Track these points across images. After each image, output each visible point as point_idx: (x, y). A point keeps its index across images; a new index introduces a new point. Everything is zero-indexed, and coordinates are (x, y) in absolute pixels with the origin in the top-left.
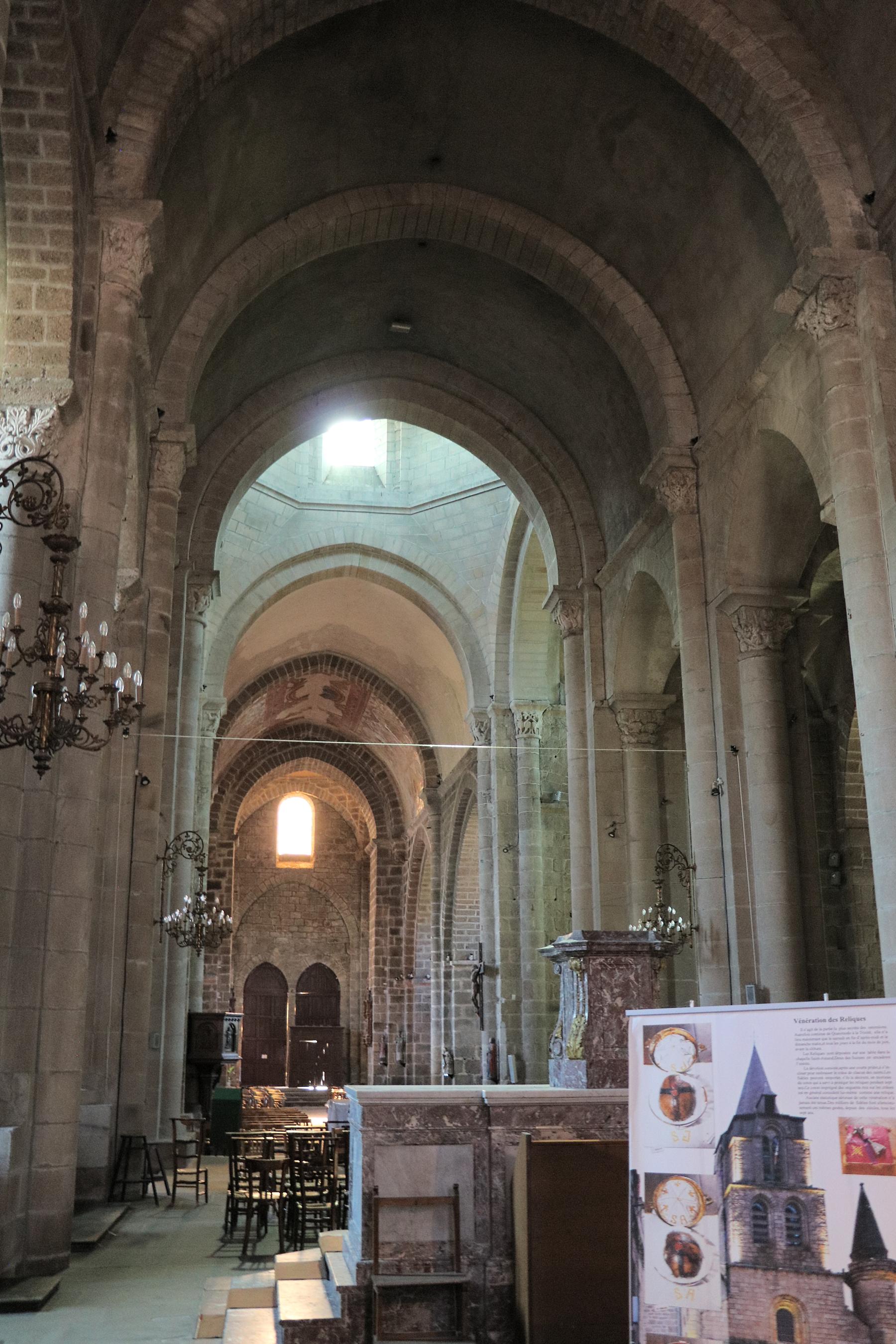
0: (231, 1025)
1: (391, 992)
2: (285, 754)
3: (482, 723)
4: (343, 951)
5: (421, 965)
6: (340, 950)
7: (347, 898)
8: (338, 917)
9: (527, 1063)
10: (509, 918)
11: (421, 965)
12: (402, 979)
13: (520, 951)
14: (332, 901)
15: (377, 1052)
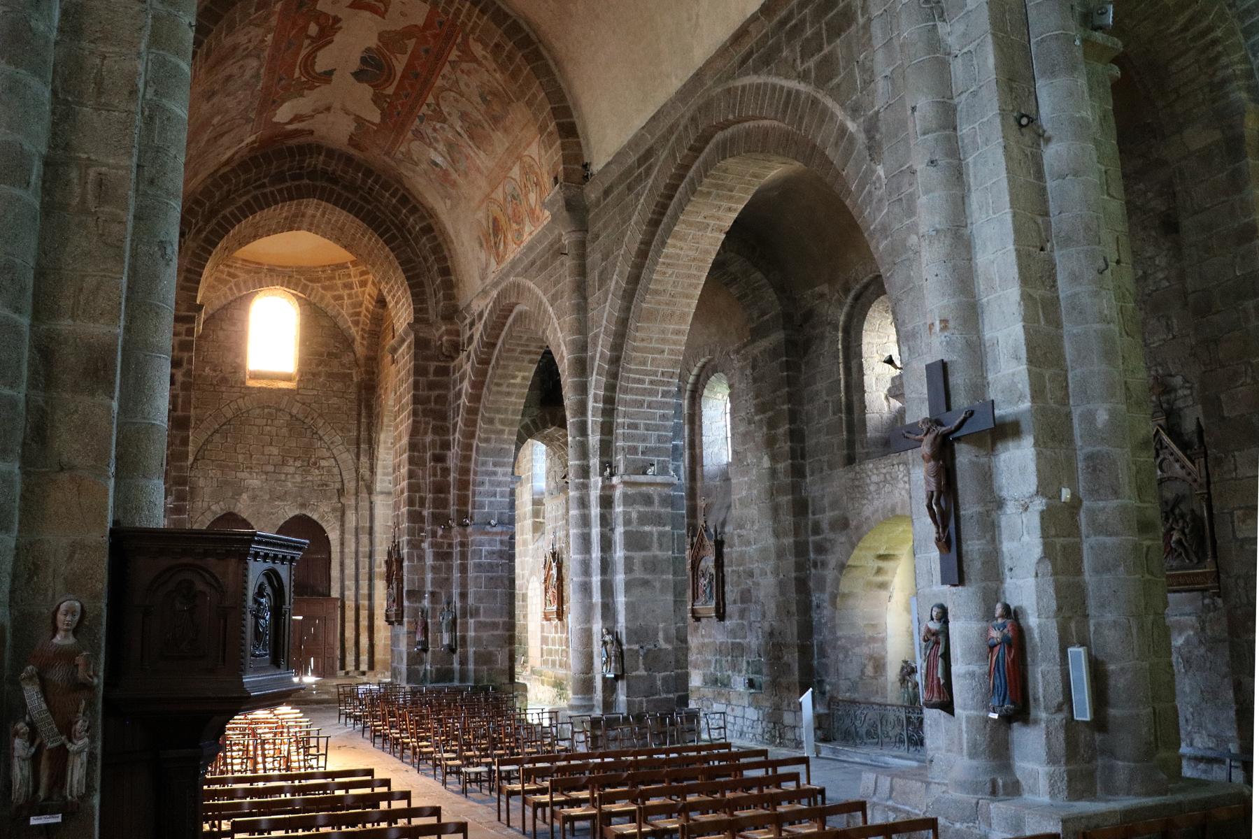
0: (271, 575)
1: (433, 545)
2: (280, 191)
4: (335, 500)
5: (482, 506)
6: (330, 499)
7: (342, 430)
8: (328, 455)
9: (1112, 667)
11: (482, 506)
12: (451, 527)
14: (321, 432)
15: (411, 633)
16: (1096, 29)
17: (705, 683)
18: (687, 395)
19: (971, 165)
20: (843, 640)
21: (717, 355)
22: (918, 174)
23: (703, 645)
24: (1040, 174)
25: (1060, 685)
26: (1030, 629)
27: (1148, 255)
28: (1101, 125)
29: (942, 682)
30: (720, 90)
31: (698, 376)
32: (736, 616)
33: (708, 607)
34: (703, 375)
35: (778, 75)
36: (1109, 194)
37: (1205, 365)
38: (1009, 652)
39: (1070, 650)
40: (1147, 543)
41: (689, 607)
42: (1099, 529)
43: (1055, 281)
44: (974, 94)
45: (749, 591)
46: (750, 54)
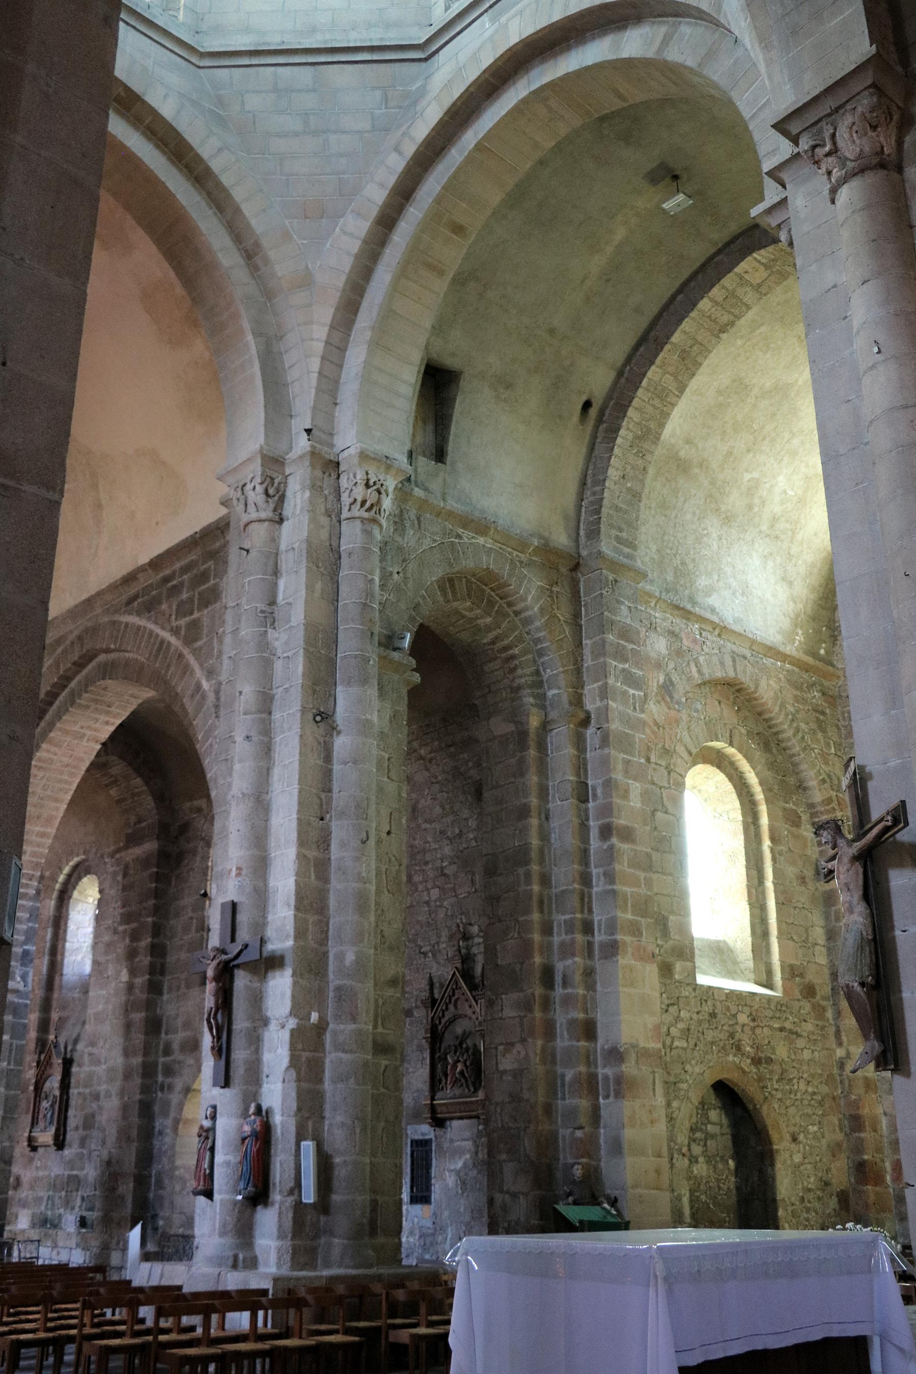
3: (272, 479)
9: (337, 1160)
10: (312, 854)
13: (328, 923)
16: (395, 649)
17: (33, 1225)
18: (55, 895)
19: (278, 744)
20: (182, 1171)
21: (91, 856)
22: (237, 745)
23: (37, 1179)
24: (328, 758)
25: (293, 1172)
26: (275, 1126)
27: (465, 816)
28: (391, 722)
29: (208, 1171)
30: (106, 619)
31: (70, 876)
32: (76, 1145)
33: (46, 1137)
34: (75, 875)
35: (156, 623)
36: (388, 777)
37: (490, 918)
38: (256, 1143)
39: (303, 1143)
40: (384, 1063)
41: (26, 1135)
42: (339, 1047)
43: (329, 845)
44: (287, 690)
45: (93, 1116)
46: (136, 597)
